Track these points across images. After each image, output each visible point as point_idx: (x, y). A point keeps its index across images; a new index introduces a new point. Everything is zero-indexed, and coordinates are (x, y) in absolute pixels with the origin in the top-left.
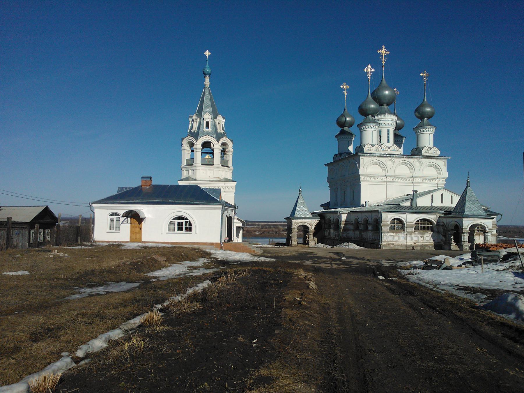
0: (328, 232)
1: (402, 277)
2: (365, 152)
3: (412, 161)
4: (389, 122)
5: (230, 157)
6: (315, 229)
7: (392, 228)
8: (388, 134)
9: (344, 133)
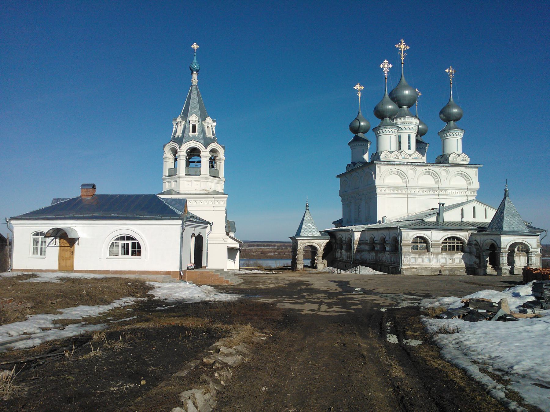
0: (339, 254)
1: (429, 340)
2: (381, 160)
3: (437, 169)
4: (410, 125)
5: (221, 166)
6: (324, 249)
7: (415, 248)
8: (409, 140)
9: (359, 139)
